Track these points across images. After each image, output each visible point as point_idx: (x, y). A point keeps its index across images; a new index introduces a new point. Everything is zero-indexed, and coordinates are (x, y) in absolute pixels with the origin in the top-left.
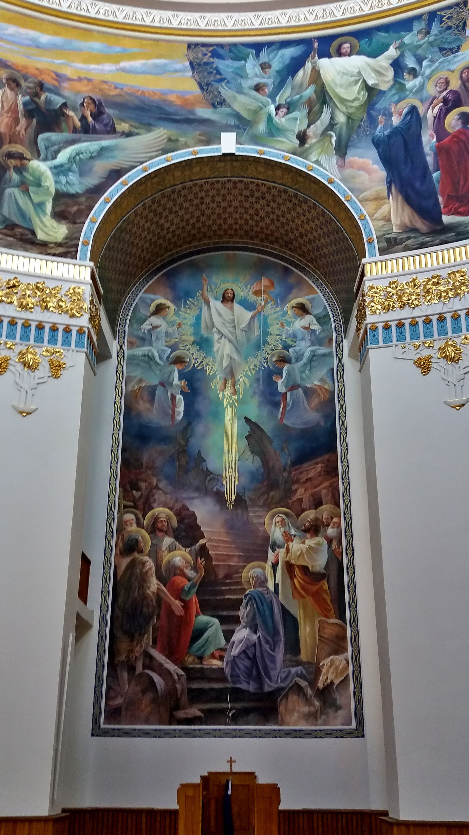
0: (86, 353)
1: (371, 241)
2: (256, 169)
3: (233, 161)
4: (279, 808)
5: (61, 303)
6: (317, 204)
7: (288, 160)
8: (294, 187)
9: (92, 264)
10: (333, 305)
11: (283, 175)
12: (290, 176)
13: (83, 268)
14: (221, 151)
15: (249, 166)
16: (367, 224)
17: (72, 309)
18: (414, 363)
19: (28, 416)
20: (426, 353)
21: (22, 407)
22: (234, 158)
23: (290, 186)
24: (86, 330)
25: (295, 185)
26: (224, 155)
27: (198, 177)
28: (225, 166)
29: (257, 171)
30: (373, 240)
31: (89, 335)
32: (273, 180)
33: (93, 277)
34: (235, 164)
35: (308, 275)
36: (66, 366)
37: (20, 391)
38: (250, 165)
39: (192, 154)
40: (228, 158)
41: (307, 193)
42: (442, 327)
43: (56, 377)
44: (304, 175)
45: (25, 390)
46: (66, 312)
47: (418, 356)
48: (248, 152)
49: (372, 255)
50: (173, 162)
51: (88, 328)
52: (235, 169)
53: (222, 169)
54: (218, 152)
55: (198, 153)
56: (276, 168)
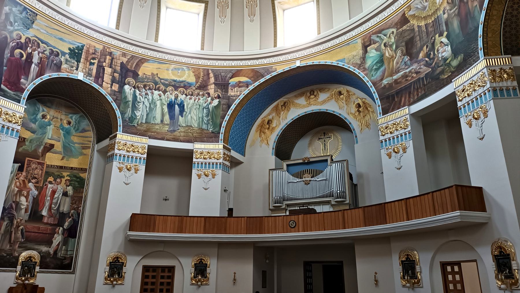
11: (496, 10)
21: (126, 182)
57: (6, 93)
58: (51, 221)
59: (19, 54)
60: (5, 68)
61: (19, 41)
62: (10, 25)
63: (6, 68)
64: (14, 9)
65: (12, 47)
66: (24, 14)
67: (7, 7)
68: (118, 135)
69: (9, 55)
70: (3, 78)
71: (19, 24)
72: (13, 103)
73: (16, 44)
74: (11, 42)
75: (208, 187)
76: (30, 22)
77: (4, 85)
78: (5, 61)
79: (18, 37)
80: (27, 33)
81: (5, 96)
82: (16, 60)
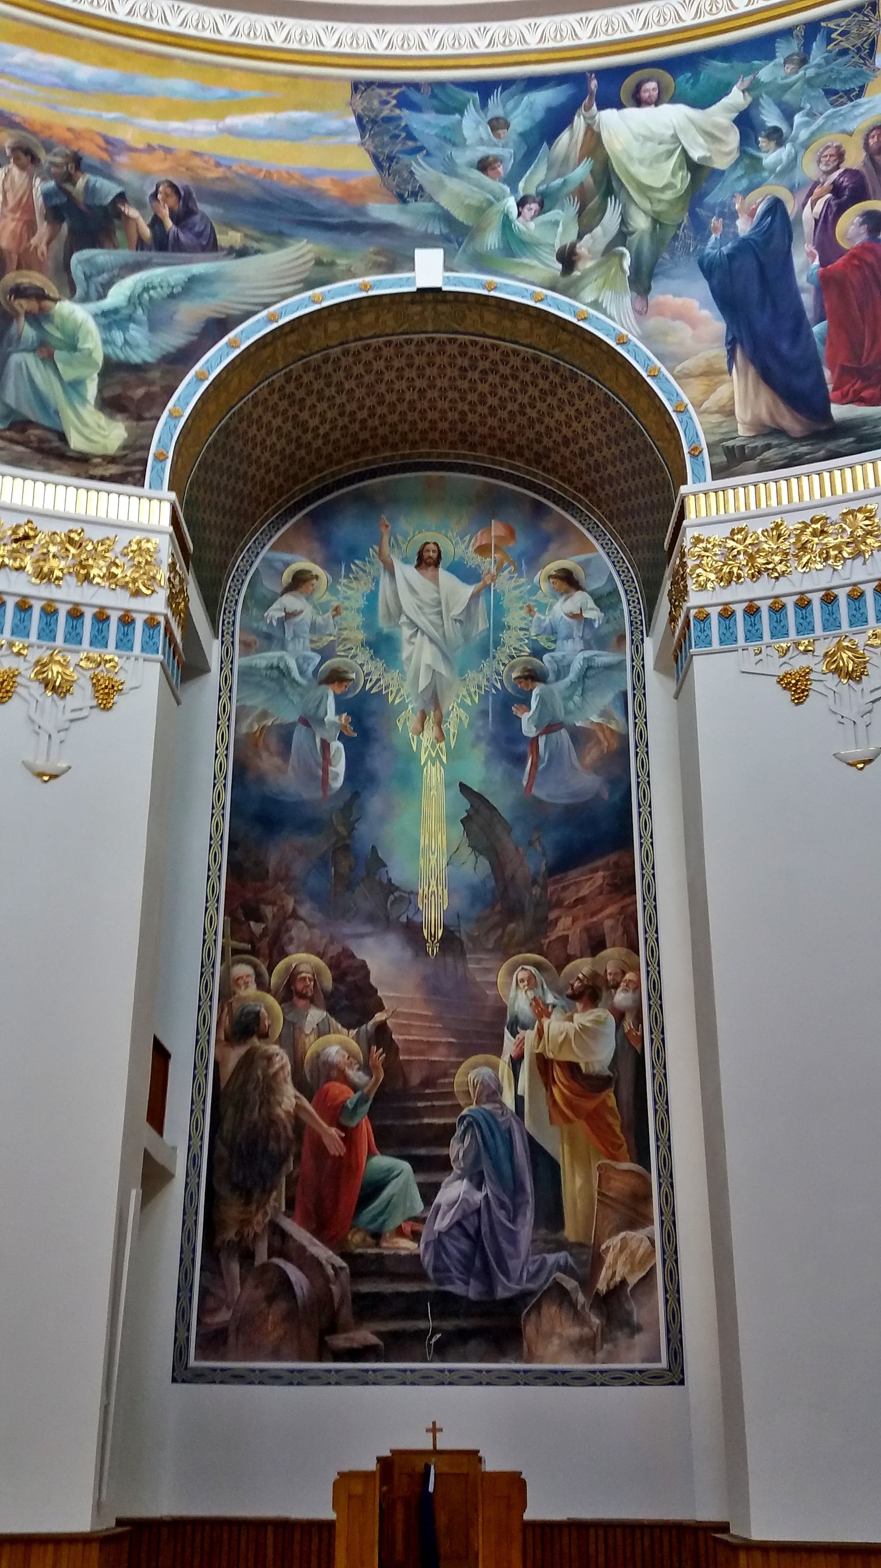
0: (161, 663)
1: (697, 453)
2: (481, 317)
3: (437, 302)
4: (525, 1518)
5: (114, 570)
6: (596, 382)
7: (541, 300)
8: (552, 352)
9: (173, 496)
10: (626, 573)
11: (532, 328)
12: (545, 330)
13: (155, 503)
14: (415, 284)
15: (467, 312)
16: (689, 421)
17: (135, 581)
18: (778, 682)
19: (52, 781)
20: (799, 662)
21: (41, 764)
22: (440, 297)
23: (545, 349)
24: (162, 619)
25: (553, 348)
26: (421, 291)
27: (371, 333)
28: (423, 312)
29: (482, 321)
30: (701, 452)
31: (168, 628)
32: (513, 339)
33: (175, 521)
34: (442, 308)
35: (578, 516)
36: (124, 686)
37: (38, 734)
38: (470, 311)
39: (361, 290)
40: (429, 297)
41: (577, 363)
42: (831, 614)
43: (106, 709)
44: (570, 328)
45: (47, 732)
46: (125, 586)
47: (786, 668)
48: (465, 286)
49: (698, 479)
50: (325, 304)
51: (166, 616)
52: (442, 317)
53: (416, 318)
54: (409, 286)
55: (372, 288)
56: (518, 315)
57: (867, 430)
58: (312, 1016)
59: (862, 224)
60: (817, 329)
61: (835, 175)
62: (772, 144)
63: (825, 323)
64: (766, 73)
65: (817, 221)
66: (817, 55)
67: (735, 89)
68: (690, 502)
69: (817, 262)
70: (827, 373)
71: (811, 108)
72: (798, 477)
73: (829, 195)
74: (804, 205)
75: (63, 765)
76: (857, 58)
77: (844, 400)
78: (807, 299)
79: (827, 164)
80: (862, 114)
81: (795, 463)
82: (856, 262)
